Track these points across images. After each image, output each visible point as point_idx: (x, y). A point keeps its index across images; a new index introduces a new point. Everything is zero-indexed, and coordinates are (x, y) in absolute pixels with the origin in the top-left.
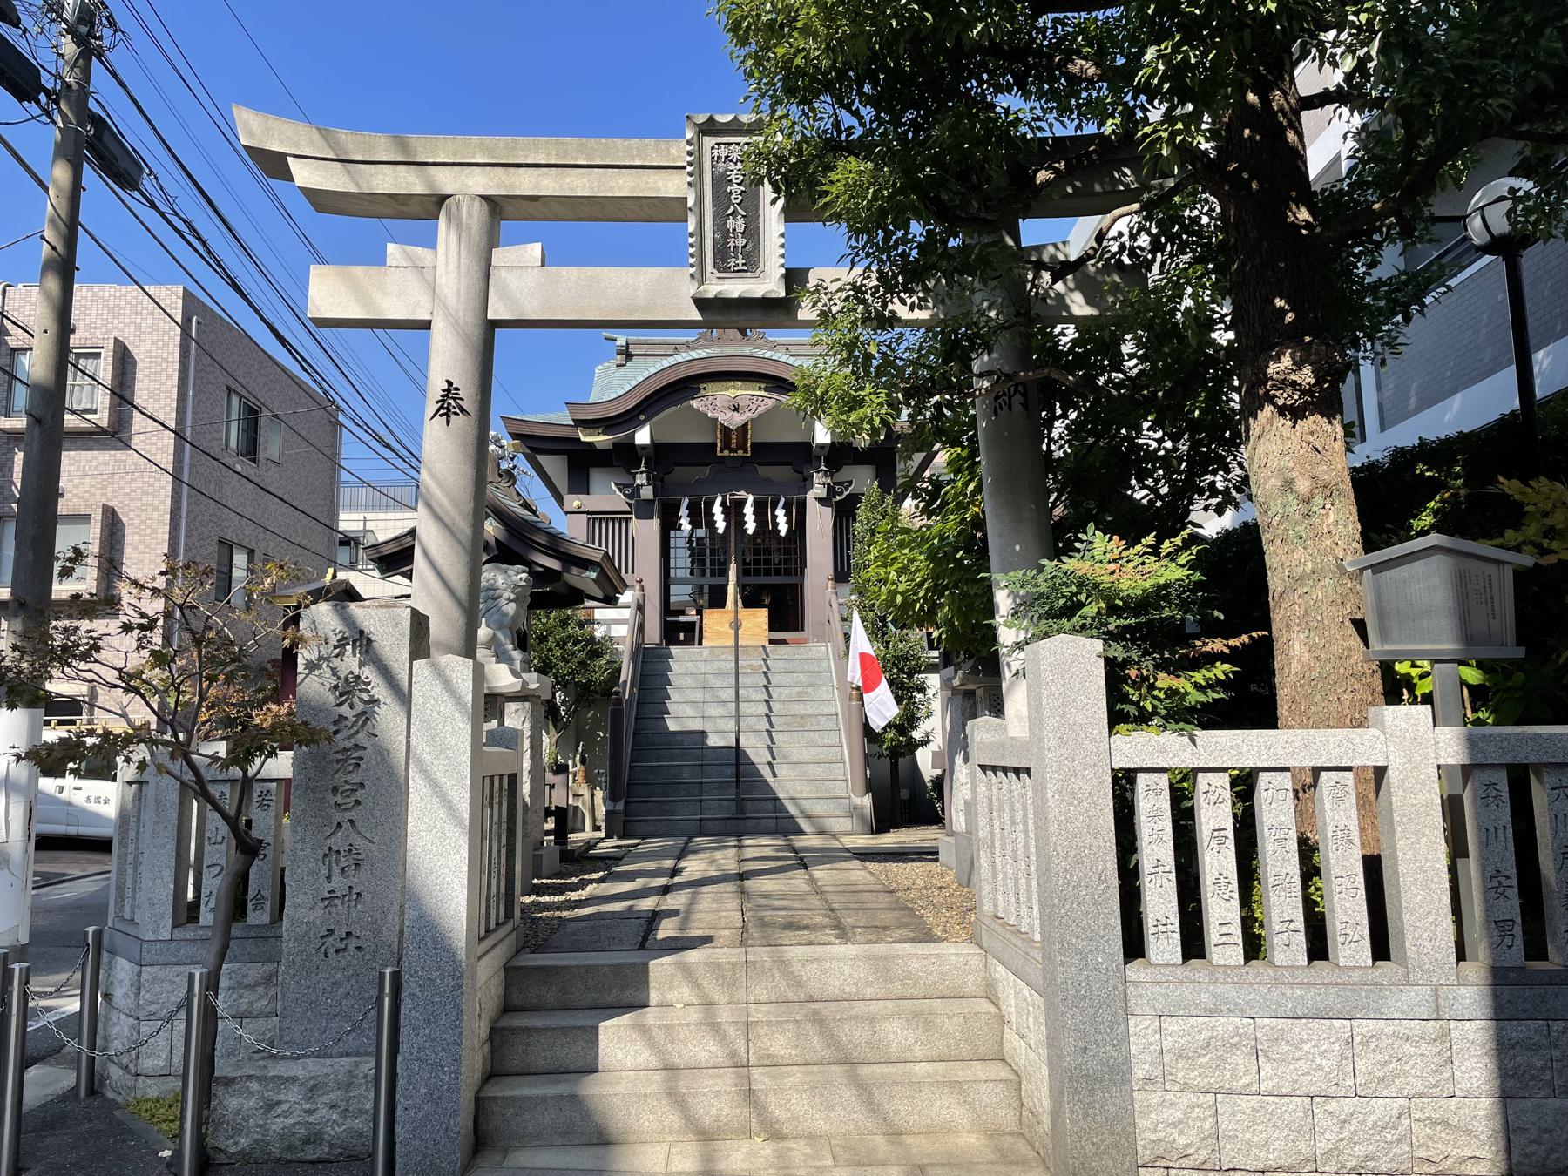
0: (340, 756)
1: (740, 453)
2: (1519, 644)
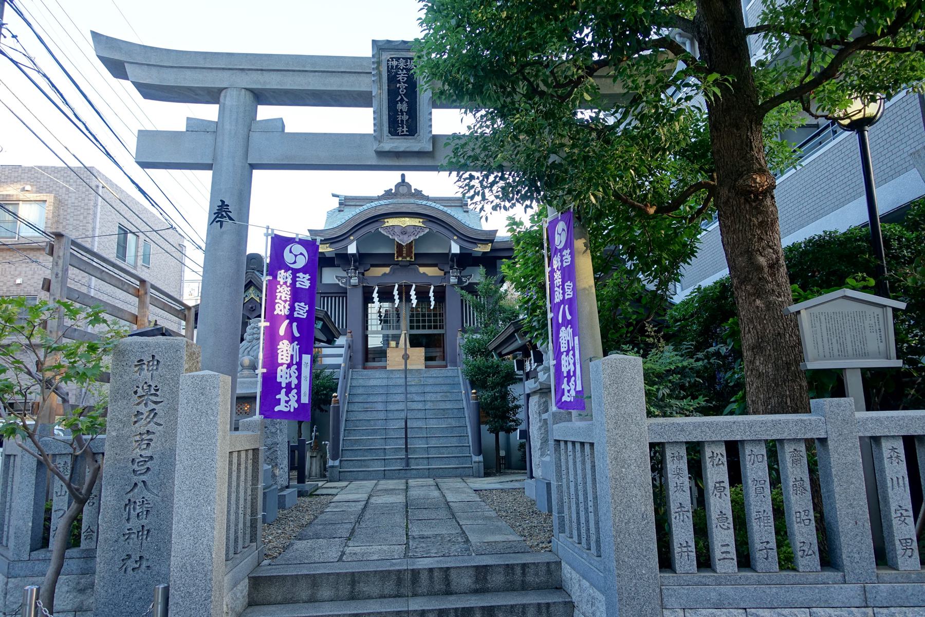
0: (138, 438)
1: (408, 259)
2: (898, 358)
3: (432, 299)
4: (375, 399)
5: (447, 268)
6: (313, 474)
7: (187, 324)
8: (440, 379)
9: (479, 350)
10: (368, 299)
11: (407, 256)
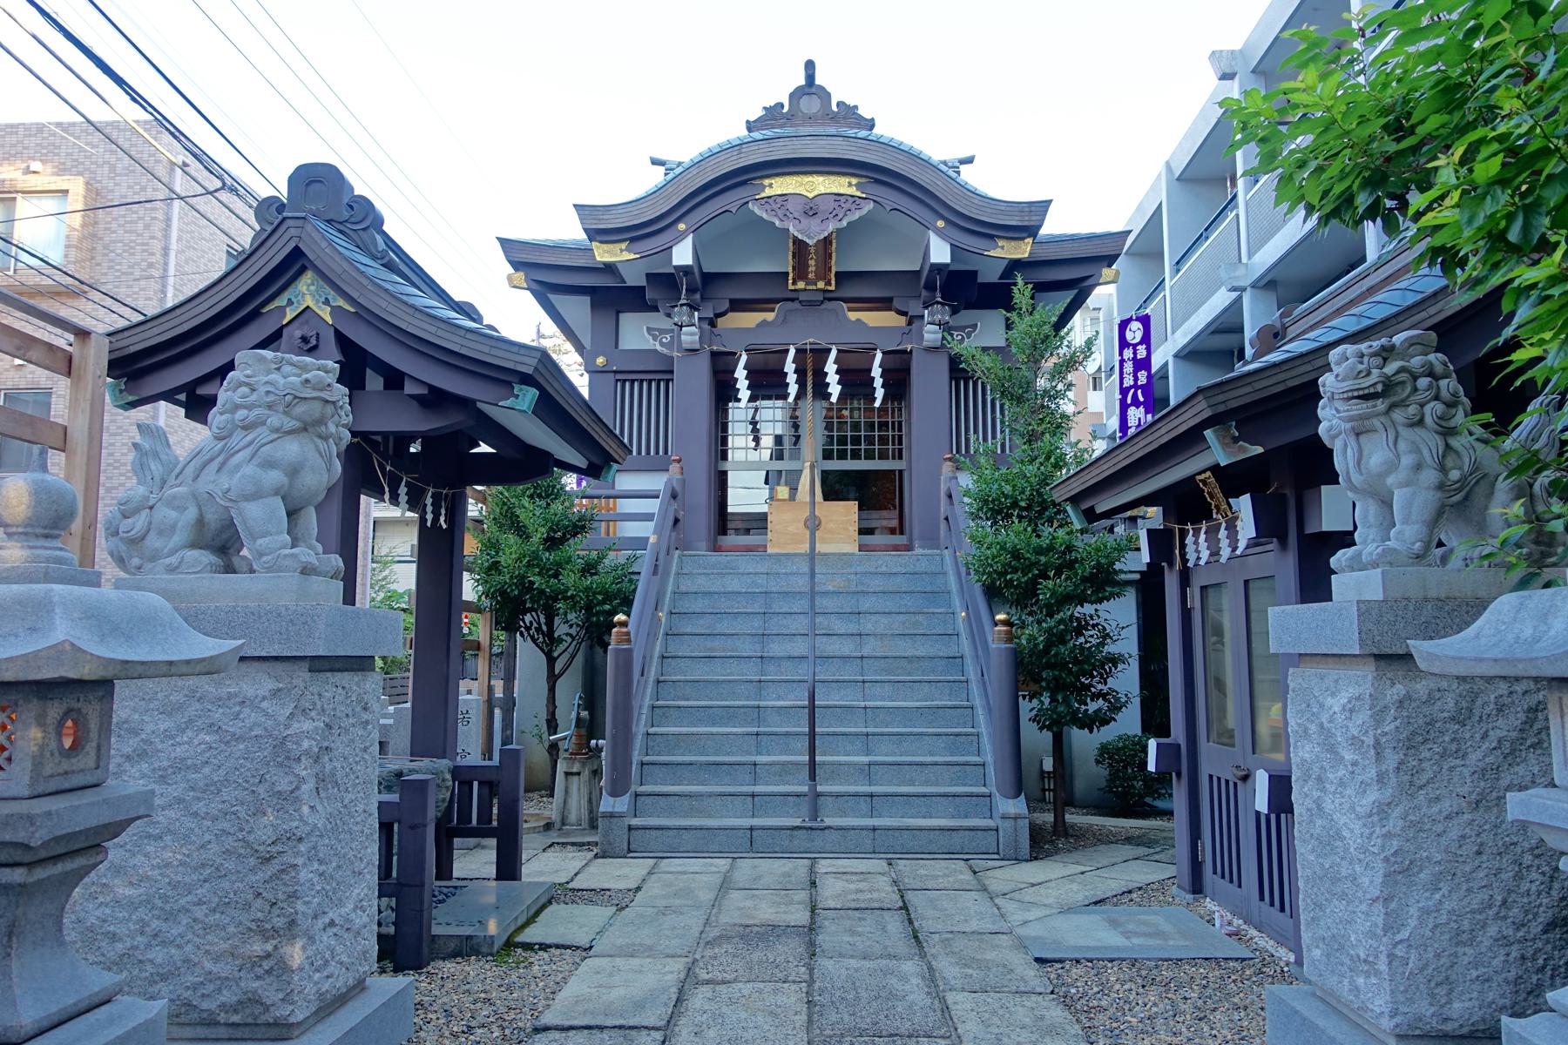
1: (821, 285)
3: (878, 383)
4: (739, 626)
5: (914, 308)
6: (573, 817)
7: (75, 388)
8: (899, 579)
9: (1015, 504)
10: (724, 392)
11: (818, 278)
